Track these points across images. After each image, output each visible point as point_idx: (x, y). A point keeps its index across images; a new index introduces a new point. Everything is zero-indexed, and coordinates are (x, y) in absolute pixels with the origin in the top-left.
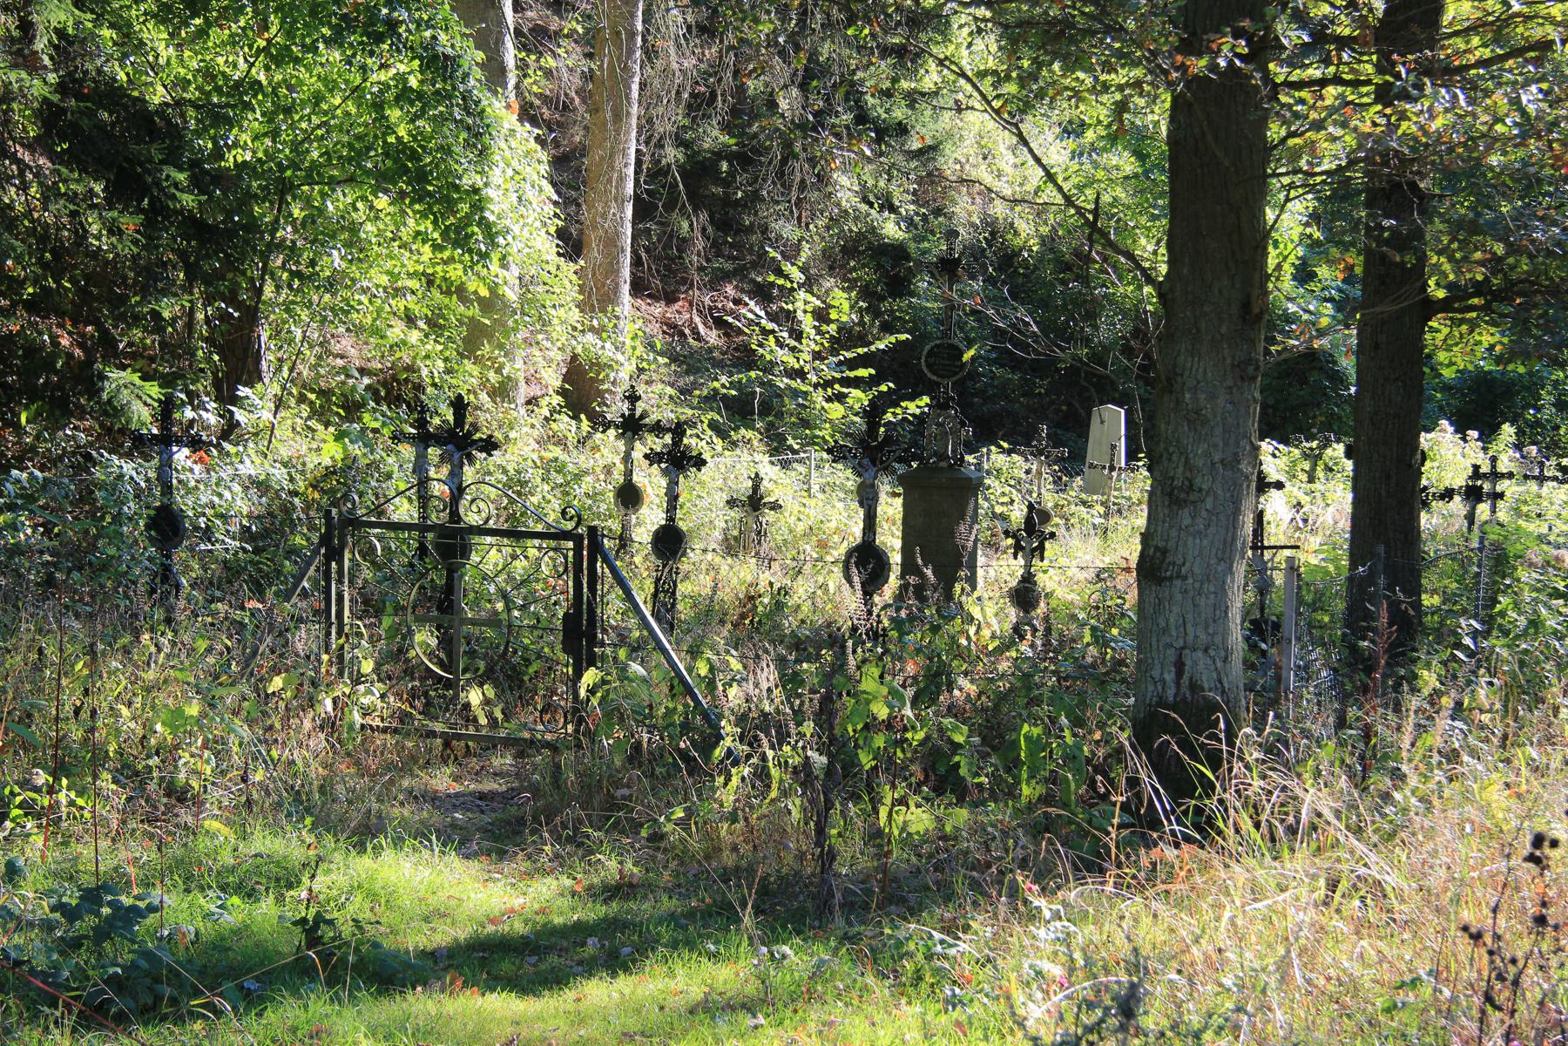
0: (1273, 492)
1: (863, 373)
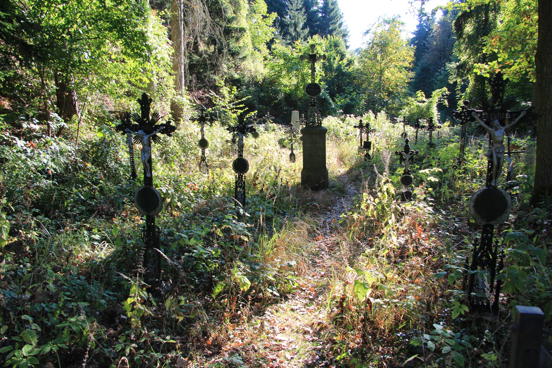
1: (241, 106)
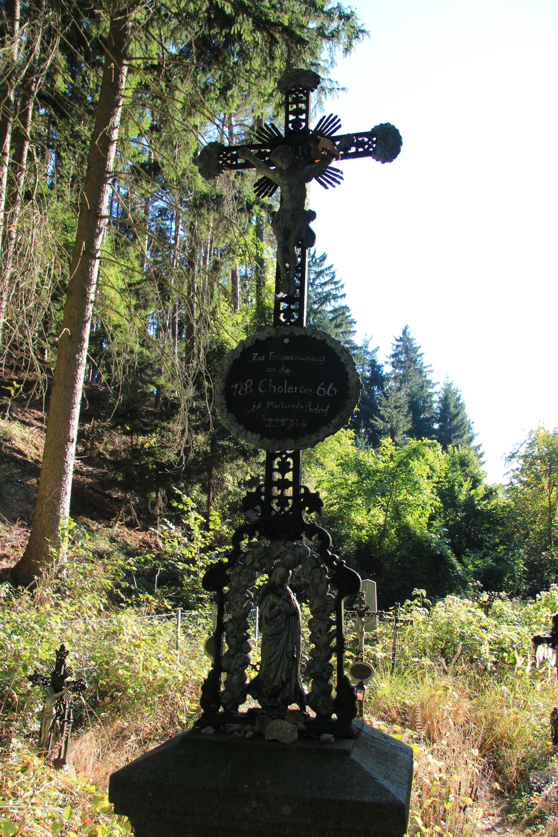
0: (355, 170)
